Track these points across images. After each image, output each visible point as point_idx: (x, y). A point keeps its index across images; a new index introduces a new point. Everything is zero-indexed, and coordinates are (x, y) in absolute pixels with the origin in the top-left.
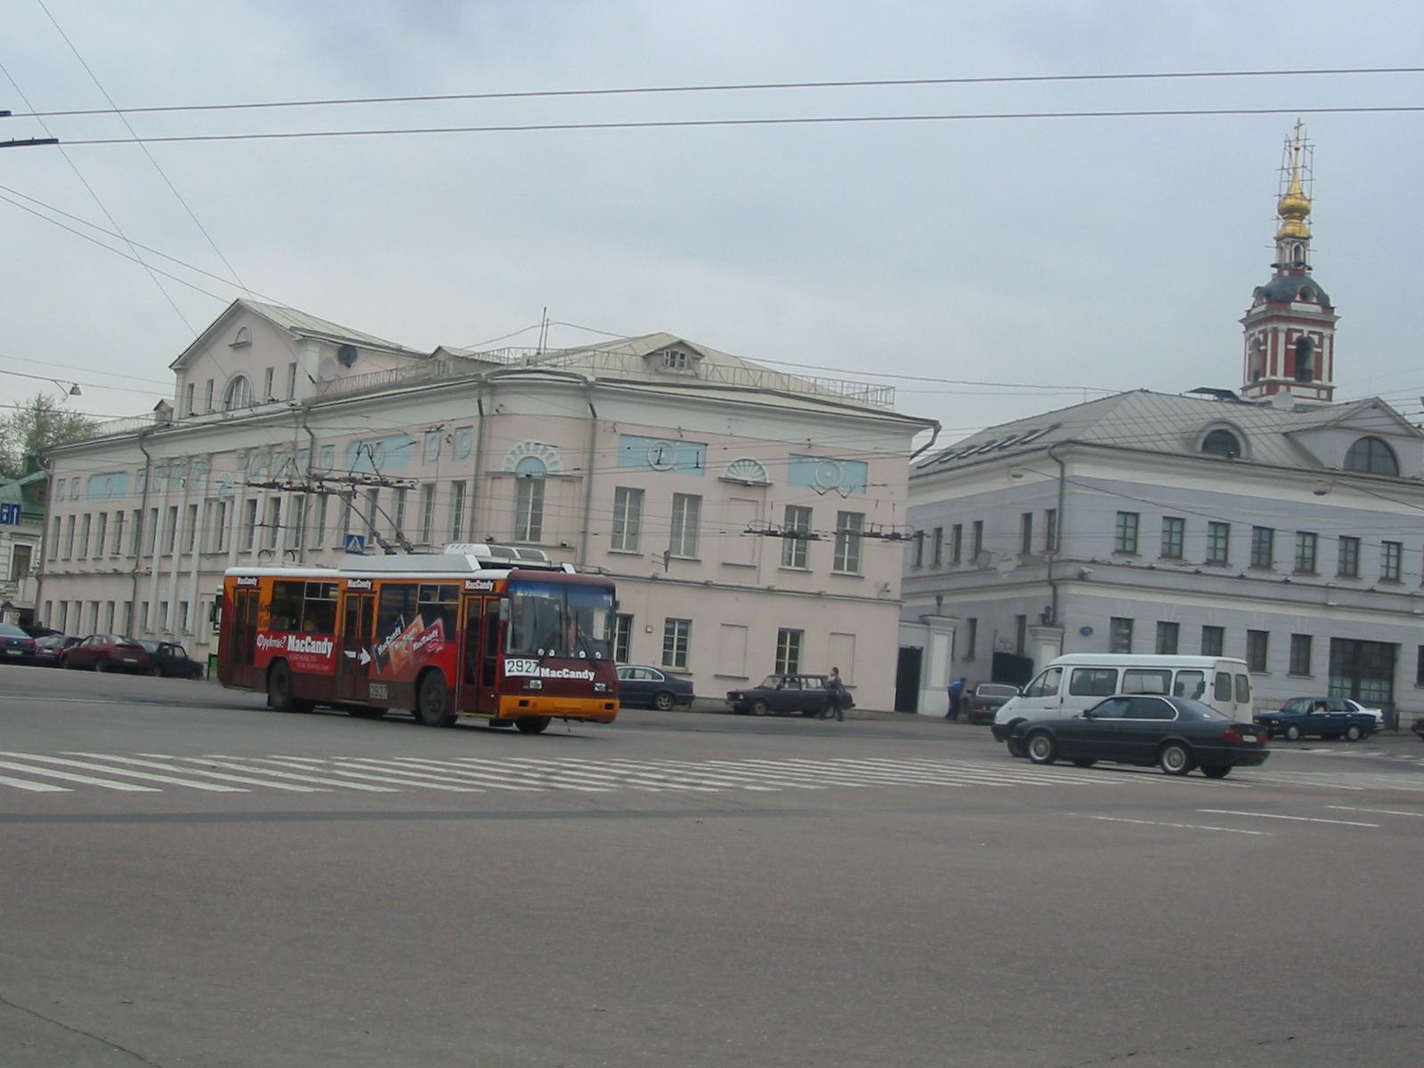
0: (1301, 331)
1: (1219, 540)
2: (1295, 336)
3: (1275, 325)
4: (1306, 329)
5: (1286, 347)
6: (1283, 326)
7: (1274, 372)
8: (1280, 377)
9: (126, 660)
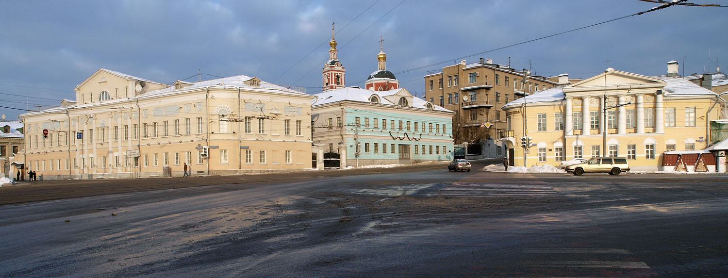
2: (336, 74)
4: (339, 73)
6: (333, 72)
7: (332, 83)
8: (333, 84)
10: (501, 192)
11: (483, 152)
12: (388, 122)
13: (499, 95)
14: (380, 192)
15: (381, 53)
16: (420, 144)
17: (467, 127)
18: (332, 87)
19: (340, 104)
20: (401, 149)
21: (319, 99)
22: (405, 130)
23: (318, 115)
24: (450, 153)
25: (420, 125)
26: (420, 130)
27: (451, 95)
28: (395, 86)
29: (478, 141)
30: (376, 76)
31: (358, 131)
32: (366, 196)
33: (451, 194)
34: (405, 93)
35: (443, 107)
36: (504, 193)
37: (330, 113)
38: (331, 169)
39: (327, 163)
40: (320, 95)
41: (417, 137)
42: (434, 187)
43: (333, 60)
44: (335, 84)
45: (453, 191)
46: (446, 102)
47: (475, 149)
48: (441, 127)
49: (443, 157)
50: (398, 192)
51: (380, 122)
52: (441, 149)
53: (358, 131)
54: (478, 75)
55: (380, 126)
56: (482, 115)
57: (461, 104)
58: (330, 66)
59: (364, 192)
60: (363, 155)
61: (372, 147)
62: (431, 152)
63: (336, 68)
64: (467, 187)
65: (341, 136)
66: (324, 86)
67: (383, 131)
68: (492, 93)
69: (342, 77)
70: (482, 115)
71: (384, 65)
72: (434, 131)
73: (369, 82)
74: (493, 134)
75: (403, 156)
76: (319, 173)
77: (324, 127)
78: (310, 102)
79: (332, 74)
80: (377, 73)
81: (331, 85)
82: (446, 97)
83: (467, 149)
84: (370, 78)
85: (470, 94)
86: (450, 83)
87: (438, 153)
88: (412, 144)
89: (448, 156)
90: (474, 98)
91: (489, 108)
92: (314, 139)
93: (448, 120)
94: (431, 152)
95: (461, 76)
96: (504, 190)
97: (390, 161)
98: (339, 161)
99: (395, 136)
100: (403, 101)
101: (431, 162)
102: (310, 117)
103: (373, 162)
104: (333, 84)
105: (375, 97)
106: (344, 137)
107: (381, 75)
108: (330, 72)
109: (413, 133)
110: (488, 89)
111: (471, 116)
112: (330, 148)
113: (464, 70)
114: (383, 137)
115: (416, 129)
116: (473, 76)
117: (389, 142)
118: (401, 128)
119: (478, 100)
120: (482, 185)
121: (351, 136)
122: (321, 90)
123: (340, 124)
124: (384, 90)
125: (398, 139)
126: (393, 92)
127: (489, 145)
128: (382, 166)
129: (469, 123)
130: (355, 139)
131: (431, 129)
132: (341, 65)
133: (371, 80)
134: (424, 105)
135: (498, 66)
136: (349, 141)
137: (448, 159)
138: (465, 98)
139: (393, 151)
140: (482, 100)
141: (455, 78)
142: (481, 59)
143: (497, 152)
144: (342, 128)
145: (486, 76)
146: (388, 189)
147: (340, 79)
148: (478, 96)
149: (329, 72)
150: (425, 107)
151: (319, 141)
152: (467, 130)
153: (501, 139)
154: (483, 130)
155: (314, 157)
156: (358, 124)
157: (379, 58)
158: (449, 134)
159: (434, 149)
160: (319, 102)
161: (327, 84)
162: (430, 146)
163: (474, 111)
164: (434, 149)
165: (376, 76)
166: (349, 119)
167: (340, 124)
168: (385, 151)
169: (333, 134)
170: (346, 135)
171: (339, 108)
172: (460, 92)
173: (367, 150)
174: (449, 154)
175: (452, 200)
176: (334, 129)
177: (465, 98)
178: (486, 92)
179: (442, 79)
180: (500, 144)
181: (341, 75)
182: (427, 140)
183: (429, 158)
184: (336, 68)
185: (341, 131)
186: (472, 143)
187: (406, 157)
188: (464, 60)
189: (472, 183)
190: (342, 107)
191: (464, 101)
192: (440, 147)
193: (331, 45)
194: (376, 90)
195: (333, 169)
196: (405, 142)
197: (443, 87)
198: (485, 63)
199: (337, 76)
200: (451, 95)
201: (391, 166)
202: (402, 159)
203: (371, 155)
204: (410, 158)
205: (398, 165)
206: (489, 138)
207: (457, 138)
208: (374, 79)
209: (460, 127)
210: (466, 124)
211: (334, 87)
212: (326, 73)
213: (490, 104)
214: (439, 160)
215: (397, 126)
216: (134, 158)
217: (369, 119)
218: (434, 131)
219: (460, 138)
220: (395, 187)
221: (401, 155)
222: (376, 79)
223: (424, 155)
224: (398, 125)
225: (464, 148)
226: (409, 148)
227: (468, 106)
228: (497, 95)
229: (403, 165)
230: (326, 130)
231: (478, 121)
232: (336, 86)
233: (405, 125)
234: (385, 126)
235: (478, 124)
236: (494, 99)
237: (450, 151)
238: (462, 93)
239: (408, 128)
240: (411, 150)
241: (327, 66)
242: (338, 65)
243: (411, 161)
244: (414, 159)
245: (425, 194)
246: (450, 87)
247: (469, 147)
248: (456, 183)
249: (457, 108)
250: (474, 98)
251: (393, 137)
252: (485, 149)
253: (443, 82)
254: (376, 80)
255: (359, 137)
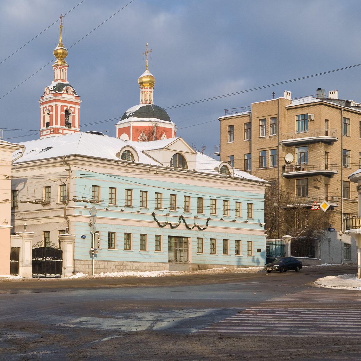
0: (67, 106)
1: (128, 202)
2: (65, 108)
3: (57, 104)
4: (69, 105)
5: (61, 113)
6: (60, 104)
7: (56, 124)
8: (59, 126)
9: (359, 254)
10: (325, 328)
11: (318, 253)
12: (151, 196)
13: (348, 153)
14: (107, 324)
15: (147, 73)
16: (207, 235)
17: (291, 209)
18: (56, 131)
19: (65, 161)
20: (173, 245)
21: (27, 151)
22: (181, 212)
23: (24, 180)
24: (259, 253)
25: (207, 203)
26: (207, 212)
27: (263, 152)
28: (168, 133)
29: (309, 233)
30: (136, 114)
31: (96, 211)
32: (82, 330)
33: (234, 330)
34: (182, 146)
35: (250, 173)
36: (328, 329)
37: (48, 177)
38: (45, 277)
39: (37, 267)
40: (29, 145)
41: (202, 224)
42: (210, 315)
43: (59, 81)
44: (61, 125)
45: (239, 325)
46: (255, 164)
47: (306, 246)
48: (244, 206)
49: (246, 260)
50: (138, 325)
51: (136, 196)
52: (244, 247)
53: (96, 211)
54: (312, 118)
55: (136, 203)
56: (318, 188)
57: (281, 168)
58: (53, 92)
59: (81, 323)
60: (104, 253)
61: (120, 240)
62: (225, 251)
63: (65, 96)
64: (268, 317)
65: (66, 217)
66: (43, 128)
67: (110, 209)
68: (335, 150)
69: (74, 113)
70: (318, 188)
71: (150, 96)
72: (232, 214)
73: (122, 124)
74: (337, 221)
75: (176, 256)
76: (23, 285)
77: (30, 202)
78: (9, 156)
79: (56, 106)
80: (136, 108)
81: (54, 126)
82: (256, 155)
83: (289, 248)
84: (125, 117)
85: (298, 150)
86: (263, 130)
87: (238, 252)
88: (193, 236)
89: (256, 258)
90: (304, 158)
91: (329, 175)
92: (17, 223)
93: (257, 195)
94: (225, 251)
95: (283, 118)
96: (331, 324)
97: (154, 264)
98: (61, 263)
99: (162, 221)
100: (179, 160)
101: (225, 268)
102: (9, 184)
103: (122, 266)
104: (59, 126)
105: (129, 151)
106: (71, 219)
107: (145, 112)
108: (53, 104)
109: (196, 218)
110: (329, 143)
111: (299, 189)
112: (45, 239)
113: (288, 109)
114: (141, 224)
115: (200, 209)
116: (304, 120)
117: (152, 231)
118: (173, 208)
119: (310, 162)
120: (296, 314)
121: (84, 220)
122: (35, 134)
123: (64, 197)
124: (149, 140)
125: (168, 226)
126: (164, 142)
127: (329, 240)
128: (138, 274)
129: (295, 201)
130: (91, 225)
131: (226, 210)
132: (74, 92)
133: (126, 120)
134: (216, 169)
135: (348, 103)
136: (80, 226)
137: (256, 264)
138: (289, 158)
139: (158, 248)
140: (318, 161)
141: (272, 122)
142: (319, 89)
143: (344, 254)
144: (67, 204)
145: (327, 121)
146: (127, 318)
147: (71, 117)
148: (311, 155)
149: (52, 104)
150: (216, 172)
151: (25, 227)
152: (291, 212)
153: (347, 231)
154: (319, 215)
155: (15, 254)
156: (95, 200)
157: (141, 83)
158: (259, 221)
159: (232, 246)
160: (27, 157)
161: (48, 125)
162: (211, 239)
163: (304, 181)
164: (232, 246)
165: (136, 114)
166: (80, 189)
167: (64, 197)
168: (143, 247)
169: (51, 214)
170: (74, 216)
171: (61, 169)
172: (280, 147)
173: (111, 244)
174: (257, 255)
175: (230, 342)
176: (53, 205)
177: (289, 158)
178: (326, 148)
179: (250, 123)
180: (347, 240)
181: (73, 109)
182: (217, 230)
183: (221, 263)
184: (65, 96)
185: (66, 209)
186: (299, 236)
187: (182, 259)
188: (289, 92)
189: (281, 309)
190: (67, 167)
191: (287, 163)
192: (229, 242)
193: (56, 54)
194: (135, 139)
195: (49, 278)
196: (181, 232)
197: (250, 138)
198: (325, 97)
199: (67, 111)
200: (263, 152)
201: (154, 274)
202: (173, 261)
203: (120, 253)
204: (187, 261)
205: (166, 272)
206: (329, 229)
207: (272, 226)
208: (132, 119)
209: (278, 208)
210: (289, 203)
211: (60, 131)
212: (47, 105)
213: (332, 169)
214: (239, 266)
215: (166, 203)
216: (316, 256)
217: (133, 192)
218: (232, 214)
219: (277, 227)
220: (139, 315)
221: (173, 254)
222: (136, 119)
223: (213, 256)
224: (168, 202)
225: (284, 246)
226: (187, 243)
227: (294, 173)
228: (345, 154)
229: (175, 273)
230: (40, 207)
231: (310, 200)
232: (63, 129)
233: (180, 203)
234: (144, 204)
235: (310, 204)
236: (339, 161)
237: (259, 250)
238: (283, 148)
239: (187, 209)
240: (190, 246)
241: (48, 92)
242: (69, 91)
243: (190, 266)
244: (195, 262)
245: (188, 329)
246: (263, 140)
247: (294, 243)
248: (252, 309)
249: (273, 174)
250: (304, 158)
251: (159, 224)
252: (322, 249)
253: (250, 129)
254: (134, 122)
255: (98, 221)
